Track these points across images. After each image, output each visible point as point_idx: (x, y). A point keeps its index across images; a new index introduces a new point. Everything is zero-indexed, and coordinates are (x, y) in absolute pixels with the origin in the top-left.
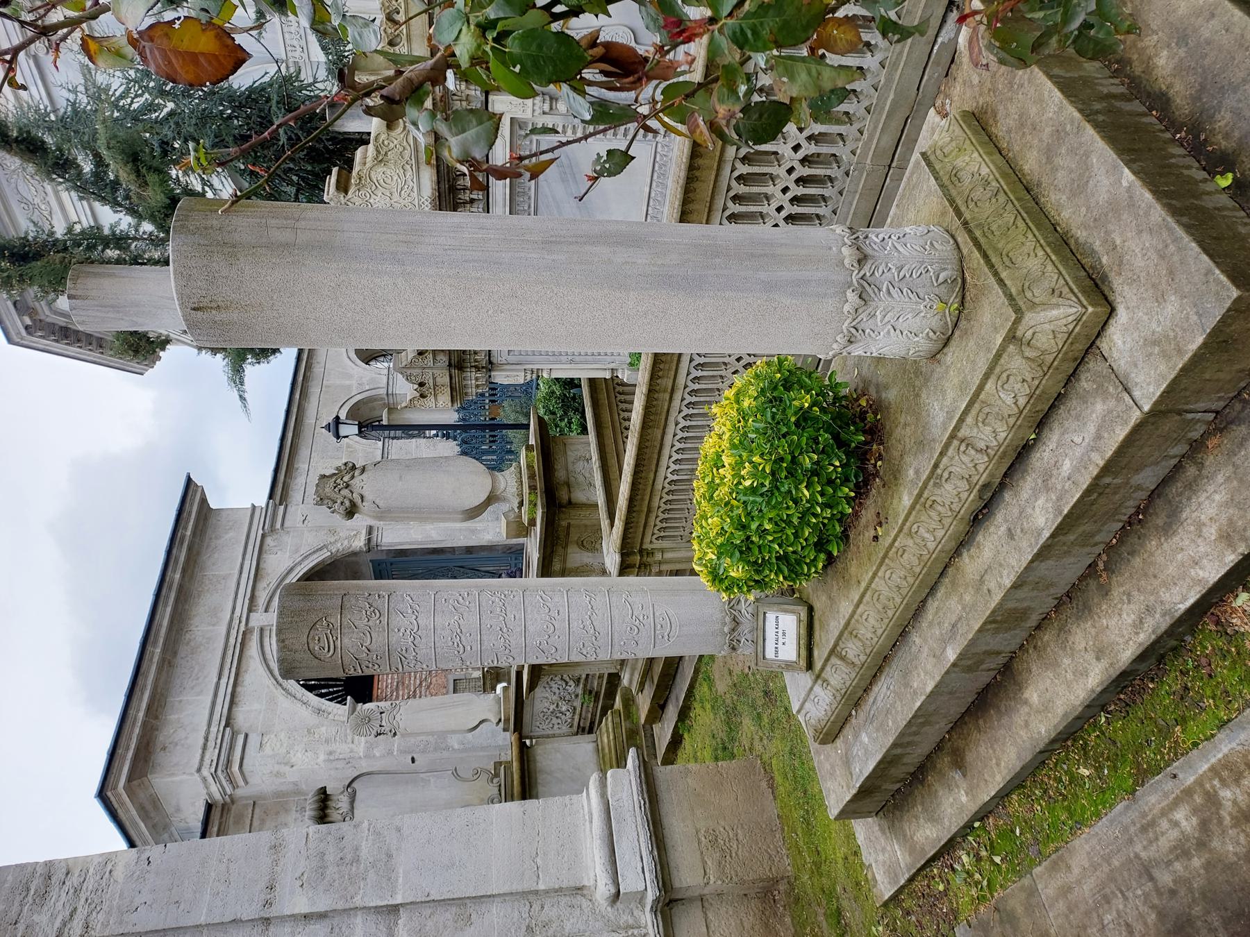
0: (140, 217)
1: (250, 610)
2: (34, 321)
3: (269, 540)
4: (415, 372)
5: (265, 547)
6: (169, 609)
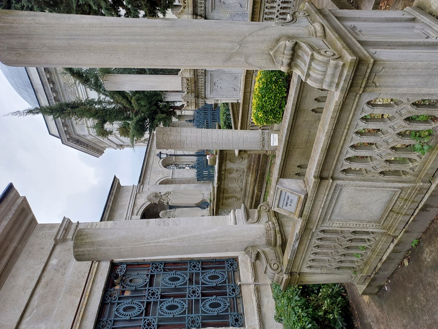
0: (107, 95)
1: (132, 215)
2: (70, 137)
3: (138, 195)
4: (186, 98)
5: (137, 197)
6: (108, 213)
